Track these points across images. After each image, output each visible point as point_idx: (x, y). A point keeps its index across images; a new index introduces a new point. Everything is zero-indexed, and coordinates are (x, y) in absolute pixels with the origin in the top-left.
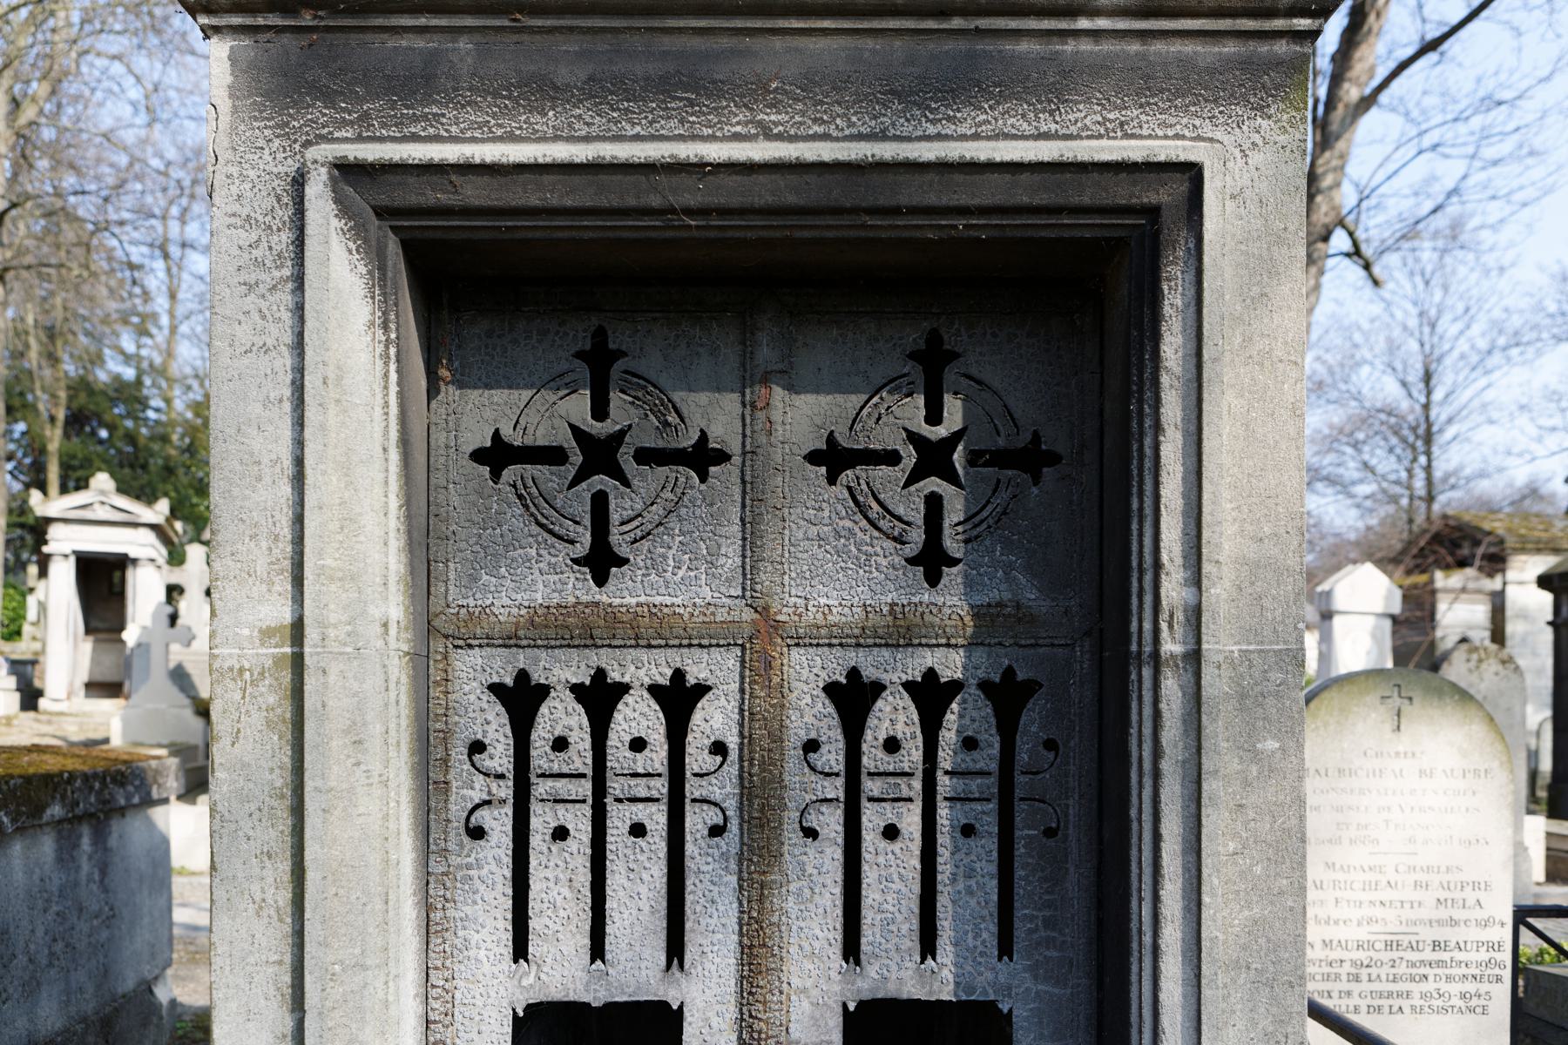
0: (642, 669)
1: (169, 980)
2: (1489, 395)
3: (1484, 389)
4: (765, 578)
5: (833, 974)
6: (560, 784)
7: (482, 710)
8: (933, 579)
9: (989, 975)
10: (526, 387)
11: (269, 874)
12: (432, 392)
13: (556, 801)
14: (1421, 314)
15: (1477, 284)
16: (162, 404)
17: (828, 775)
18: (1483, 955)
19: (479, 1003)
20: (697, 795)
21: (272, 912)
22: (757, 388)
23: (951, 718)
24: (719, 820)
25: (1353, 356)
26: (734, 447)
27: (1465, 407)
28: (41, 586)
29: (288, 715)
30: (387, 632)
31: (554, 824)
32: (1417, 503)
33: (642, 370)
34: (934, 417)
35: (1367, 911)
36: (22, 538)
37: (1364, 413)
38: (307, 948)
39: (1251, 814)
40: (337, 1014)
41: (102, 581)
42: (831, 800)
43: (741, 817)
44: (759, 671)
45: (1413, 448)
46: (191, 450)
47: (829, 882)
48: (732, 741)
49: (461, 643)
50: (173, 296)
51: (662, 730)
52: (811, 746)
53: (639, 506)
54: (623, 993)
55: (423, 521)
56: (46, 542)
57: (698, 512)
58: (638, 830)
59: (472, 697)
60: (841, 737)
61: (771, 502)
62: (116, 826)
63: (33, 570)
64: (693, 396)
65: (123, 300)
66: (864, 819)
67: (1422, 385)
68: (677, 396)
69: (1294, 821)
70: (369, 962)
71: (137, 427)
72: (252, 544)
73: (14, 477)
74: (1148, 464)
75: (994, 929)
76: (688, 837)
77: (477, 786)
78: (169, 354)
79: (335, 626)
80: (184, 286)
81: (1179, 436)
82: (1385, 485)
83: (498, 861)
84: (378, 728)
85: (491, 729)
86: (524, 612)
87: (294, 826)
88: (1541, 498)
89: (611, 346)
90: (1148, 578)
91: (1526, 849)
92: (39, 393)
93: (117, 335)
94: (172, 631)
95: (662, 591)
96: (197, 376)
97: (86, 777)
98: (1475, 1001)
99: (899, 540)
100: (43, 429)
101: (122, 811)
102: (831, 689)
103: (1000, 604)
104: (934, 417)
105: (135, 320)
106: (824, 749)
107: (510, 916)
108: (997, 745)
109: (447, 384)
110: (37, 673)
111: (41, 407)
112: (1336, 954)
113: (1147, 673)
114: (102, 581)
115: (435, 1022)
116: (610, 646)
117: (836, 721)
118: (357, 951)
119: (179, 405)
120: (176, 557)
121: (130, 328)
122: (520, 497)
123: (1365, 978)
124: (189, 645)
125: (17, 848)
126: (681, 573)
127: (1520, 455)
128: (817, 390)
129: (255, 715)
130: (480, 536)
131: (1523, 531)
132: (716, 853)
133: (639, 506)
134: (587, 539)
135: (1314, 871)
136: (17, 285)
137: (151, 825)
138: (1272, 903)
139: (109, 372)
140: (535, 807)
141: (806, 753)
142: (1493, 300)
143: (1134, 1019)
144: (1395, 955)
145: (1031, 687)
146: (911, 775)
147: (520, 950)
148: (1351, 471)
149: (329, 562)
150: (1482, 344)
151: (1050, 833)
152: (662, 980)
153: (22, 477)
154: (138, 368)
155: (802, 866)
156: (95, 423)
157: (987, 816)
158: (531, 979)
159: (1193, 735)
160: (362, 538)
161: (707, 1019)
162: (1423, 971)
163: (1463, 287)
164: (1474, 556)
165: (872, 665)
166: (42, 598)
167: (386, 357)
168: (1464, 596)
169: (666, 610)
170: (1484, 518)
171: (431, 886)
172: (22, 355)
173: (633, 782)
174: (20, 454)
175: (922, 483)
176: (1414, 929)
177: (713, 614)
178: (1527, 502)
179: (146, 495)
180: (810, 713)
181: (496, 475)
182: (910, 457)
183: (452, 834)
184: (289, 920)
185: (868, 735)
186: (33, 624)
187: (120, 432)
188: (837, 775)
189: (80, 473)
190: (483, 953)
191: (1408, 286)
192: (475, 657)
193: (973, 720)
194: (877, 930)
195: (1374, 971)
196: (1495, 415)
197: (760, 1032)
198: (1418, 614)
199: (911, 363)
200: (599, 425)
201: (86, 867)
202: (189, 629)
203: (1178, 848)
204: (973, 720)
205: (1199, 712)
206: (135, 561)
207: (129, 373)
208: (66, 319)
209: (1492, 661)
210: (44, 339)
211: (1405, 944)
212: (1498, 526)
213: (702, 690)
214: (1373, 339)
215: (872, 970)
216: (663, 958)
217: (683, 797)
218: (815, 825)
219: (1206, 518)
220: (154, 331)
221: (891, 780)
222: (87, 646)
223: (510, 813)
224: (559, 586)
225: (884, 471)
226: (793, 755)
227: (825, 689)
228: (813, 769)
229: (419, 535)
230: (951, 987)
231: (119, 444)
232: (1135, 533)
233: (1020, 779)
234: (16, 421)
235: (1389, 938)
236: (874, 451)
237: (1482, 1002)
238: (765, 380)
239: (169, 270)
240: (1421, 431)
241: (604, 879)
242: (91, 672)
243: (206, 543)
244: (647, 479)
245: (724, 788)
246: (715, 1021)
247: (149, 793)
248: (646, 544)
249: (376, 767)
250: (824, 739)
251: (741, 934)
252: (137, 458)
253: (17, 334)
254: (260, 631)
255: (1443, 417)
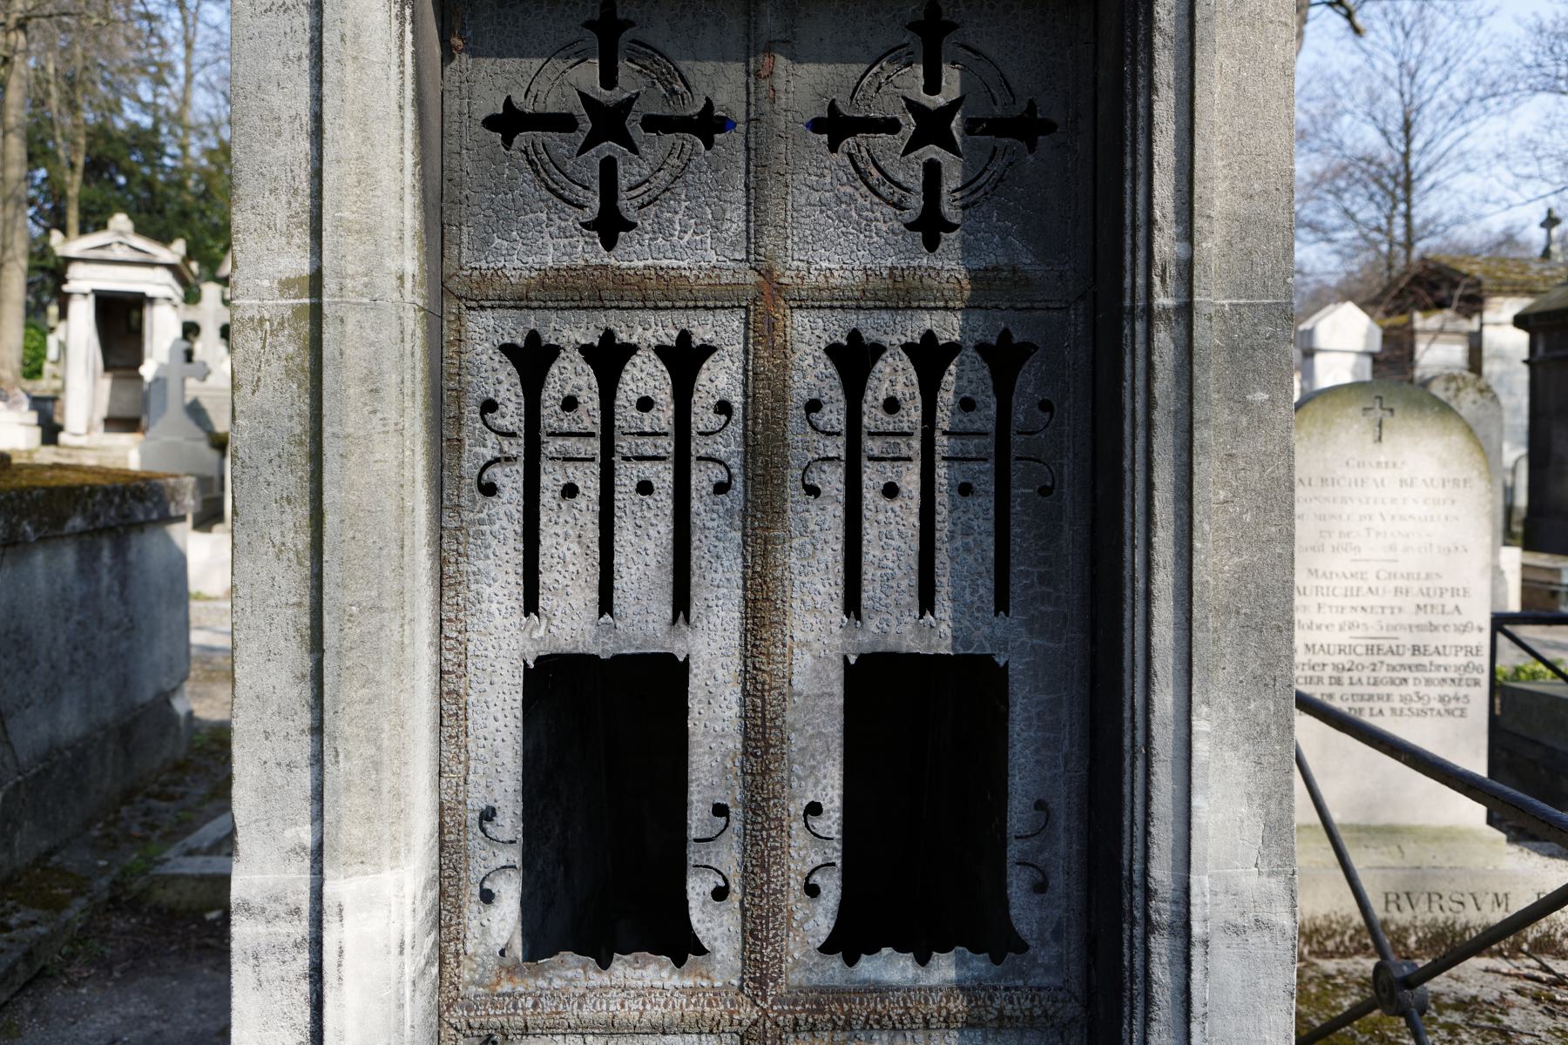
0: (649, 330)
1: (187, 696)
2: (1467, 144)
3: (1461, 139)
4: (769, 241)
5: (835, 628)
6: (569, 443)
7: (494, 370)
8: (931, 244)
9: (986, 630)
10: (538, 56)
11: (288, 518)
12: (448, 54)
13: (565, 459)
14: (1401, 65)
15: (1456, 35)
16: (177, 151)
17: (829, 434)
18: (1462, 660)
19: (492, 655)
20: (702, 452)
21: (291, 555)
22: (761, 57)
23: (949, 380)
24: (724, 477)
25: (1334, 106)
26: (739, 114)
27: (1443, 155)
28: (61, 327)
29: (307, 365)
30: (402, 285)
31: (563, 482)
32: (1397, 248)
33: (650, 40)
34: (933, 86)
35: (1349, 617)
36: (43, 281)
37: (1345, 161)
38: (326, 589)
39: (1241, 464)
40: (354, 654)
41: (120, 319)
42: (832, 459)
43: (746, 475)
44: (763, 334)
45: (1393, 195)
46: (206, 195)
47: (830, 538)
48: (737, 401)
49: (473, 304)
50: (189, 46)
51: (669, 390)
52: (813, 406)
53: (646, 172)
54: (631, 645)
55: (438, 184)
56: (66, 281)
57: (704, 177)
58: (645, 488)
59: (484, 358)
60: (842, 398)
61: (775, 168)
62: (135, 540)
63: (53, 310)
64: (699, 65)
65: (139, 48)
66: (865, 477)
67: (1401, 135)
68: (684, 65)
69: (1283, 471)
70: (385, 605)
71: (154, 173)
72: (272, 198)
73: (36, 222)
74: (1141, 123)
75: (991, 584)
76: (694, 494)
77: (489, 444)
78: (185, 102)
79: (353, 277)
80: (198, 39)
81: (1172, 94)
82: (1365, 230)
83: (509, 517)
84: (394, 378)
85: (503, 388)
86: (534, 274)
87: (313, 472)
88: (1517, 244)
89: (620, 16)
90: (1141, 234)
91: (1502, 573)
92: (59, 140)
93: (134, 83)
94: (189, 366)
95: (669, 254)
96: (212, 122)
97: (107, 492)
98: (1453, 705)
99: (899, 206)
100: (62, 174)
101: (141, 526)
102: (833, 351)
103: (996, 269)
104: (933, 86)
105: (152, 69)
106: (826, 409)
107: (520, 571)
108: (994, 407)
109: (460, 52)
110: (57, 410)
111: (61, 153)
112: (1318, 658)
113: (1140, 327)
114: (120, 319)
115: (449, 672)
116: (618, 308)
117: (837, 382)
118: (374, 593)
119: (194, 151)
120: (192, 296)
121: (146, 78)
122: (531, 162)
123: (1346, 681)
124: (204, 379)
125: (39, 558)
126: (687, 237)
127: (1497, 202)
128: (819, 60)
129: (275, 363)
130: (492, 201)
131: (1500, 274)
132: (721, 509)
133: (646, 172)
134: (596, 203)
135: (1300, 578)
136: (37, 34)
137: (169, 541)
138: (1261, 550)
139: (127, 121)
140: (546, 465)
141: (808, 413)
142: (1471, 51)
143: (1127, 663)
144: (1376, 659)
145: (1026, 350)
146: (909, 435)
147: (531, 604)
148: (1332, 217)
149: (346, 214)
150: (1461, 94)
151: (1045, 491)
152: (668, 633)
153: (42, 222)
154: (155, 116)
155: (804, 523)
156: (113, 170)
157: (984, 475)
158: (541, 632)
159: (1185, 386)
160: (379, 193)
161: (712, 671)
162: (1403, 674)
163: (1442, 39)
164: (1451, 297)
165: (872, 327)
166: (62, 338)
167: (401, 17)
168: (1442, 337)
169: (672, 273)
170: (1462, 261)
171: (445, 540)
172: (43, 103)
173: (640, 441)
174: (40, 201)
175: (921, 151)
176: (1393, 634)
177: (718, 276)
178: (1504, 250)
179: (165, 239)
180: (810, 373)
181: (507, 142)
182: (909, 125)
183: (465, 491)
184: (308, 563)
185: (869, 396)
186: (53, 362)
187: (138, 179)
188: (838, 434)
189: (98, 218)
190: (494, 606)
191: (1389, 38)
192: (488, 319)
193: (971, 382)
194: (877, 585)
195: (1355, 675)
196: (1473, 163)
197: (763, 684)
198: (1398, 353)
199: (910, 34)
200: (607, 93)
201: (106, 579)
202: (204, 364)
203: (1170, 496)
204: (971, 382)
205: (1191, 363)
206: (152, 300)
207: (146, 121)
208: (86, 68)
209: (1470, 390)
210: (65, 87)
211: (1386, 648)
212: (1476, 270)
213: (707, 351)
214: (1354, 88)
215: (873, 625)
216: (670, 612)
217: (690, 455)
218: (817, 483)
219: (1198, 174)
220: (170, 80)
221: (891, 440)
222: (106, 383)
223: (521, 470)
224: (569, 249)
225: (883, 138)
226: (796, 415)
227: (827, 351)
228: (815, 428)
229: (433, 197)
230: (949, 641)
231: (137, 190)
232: (1128, 191)
233: (1016, 439)
234: (37, 168)
235: (1370, 642)
236: (875, 120)
237: (1461, 705)
238: (769, 49)
239: (184, 20)
240: (1401, 178)
241: (612, 535)
242: (110, 407)
243: (225, 281)
244: (655, 147)
245: (728, 446)
246: (720, 673)
247: (167, 510)
248: (653, 209)
249: (393, 416)
250: (825, 399)
251: (745, 588)
252: (153, 203)
253: (38, 82)
254: (280, 282)
255: (1422, 166)
